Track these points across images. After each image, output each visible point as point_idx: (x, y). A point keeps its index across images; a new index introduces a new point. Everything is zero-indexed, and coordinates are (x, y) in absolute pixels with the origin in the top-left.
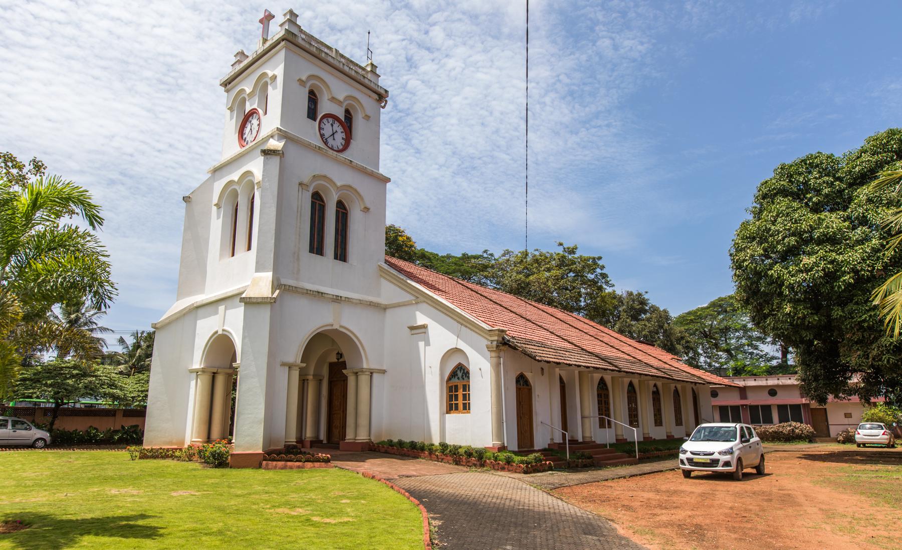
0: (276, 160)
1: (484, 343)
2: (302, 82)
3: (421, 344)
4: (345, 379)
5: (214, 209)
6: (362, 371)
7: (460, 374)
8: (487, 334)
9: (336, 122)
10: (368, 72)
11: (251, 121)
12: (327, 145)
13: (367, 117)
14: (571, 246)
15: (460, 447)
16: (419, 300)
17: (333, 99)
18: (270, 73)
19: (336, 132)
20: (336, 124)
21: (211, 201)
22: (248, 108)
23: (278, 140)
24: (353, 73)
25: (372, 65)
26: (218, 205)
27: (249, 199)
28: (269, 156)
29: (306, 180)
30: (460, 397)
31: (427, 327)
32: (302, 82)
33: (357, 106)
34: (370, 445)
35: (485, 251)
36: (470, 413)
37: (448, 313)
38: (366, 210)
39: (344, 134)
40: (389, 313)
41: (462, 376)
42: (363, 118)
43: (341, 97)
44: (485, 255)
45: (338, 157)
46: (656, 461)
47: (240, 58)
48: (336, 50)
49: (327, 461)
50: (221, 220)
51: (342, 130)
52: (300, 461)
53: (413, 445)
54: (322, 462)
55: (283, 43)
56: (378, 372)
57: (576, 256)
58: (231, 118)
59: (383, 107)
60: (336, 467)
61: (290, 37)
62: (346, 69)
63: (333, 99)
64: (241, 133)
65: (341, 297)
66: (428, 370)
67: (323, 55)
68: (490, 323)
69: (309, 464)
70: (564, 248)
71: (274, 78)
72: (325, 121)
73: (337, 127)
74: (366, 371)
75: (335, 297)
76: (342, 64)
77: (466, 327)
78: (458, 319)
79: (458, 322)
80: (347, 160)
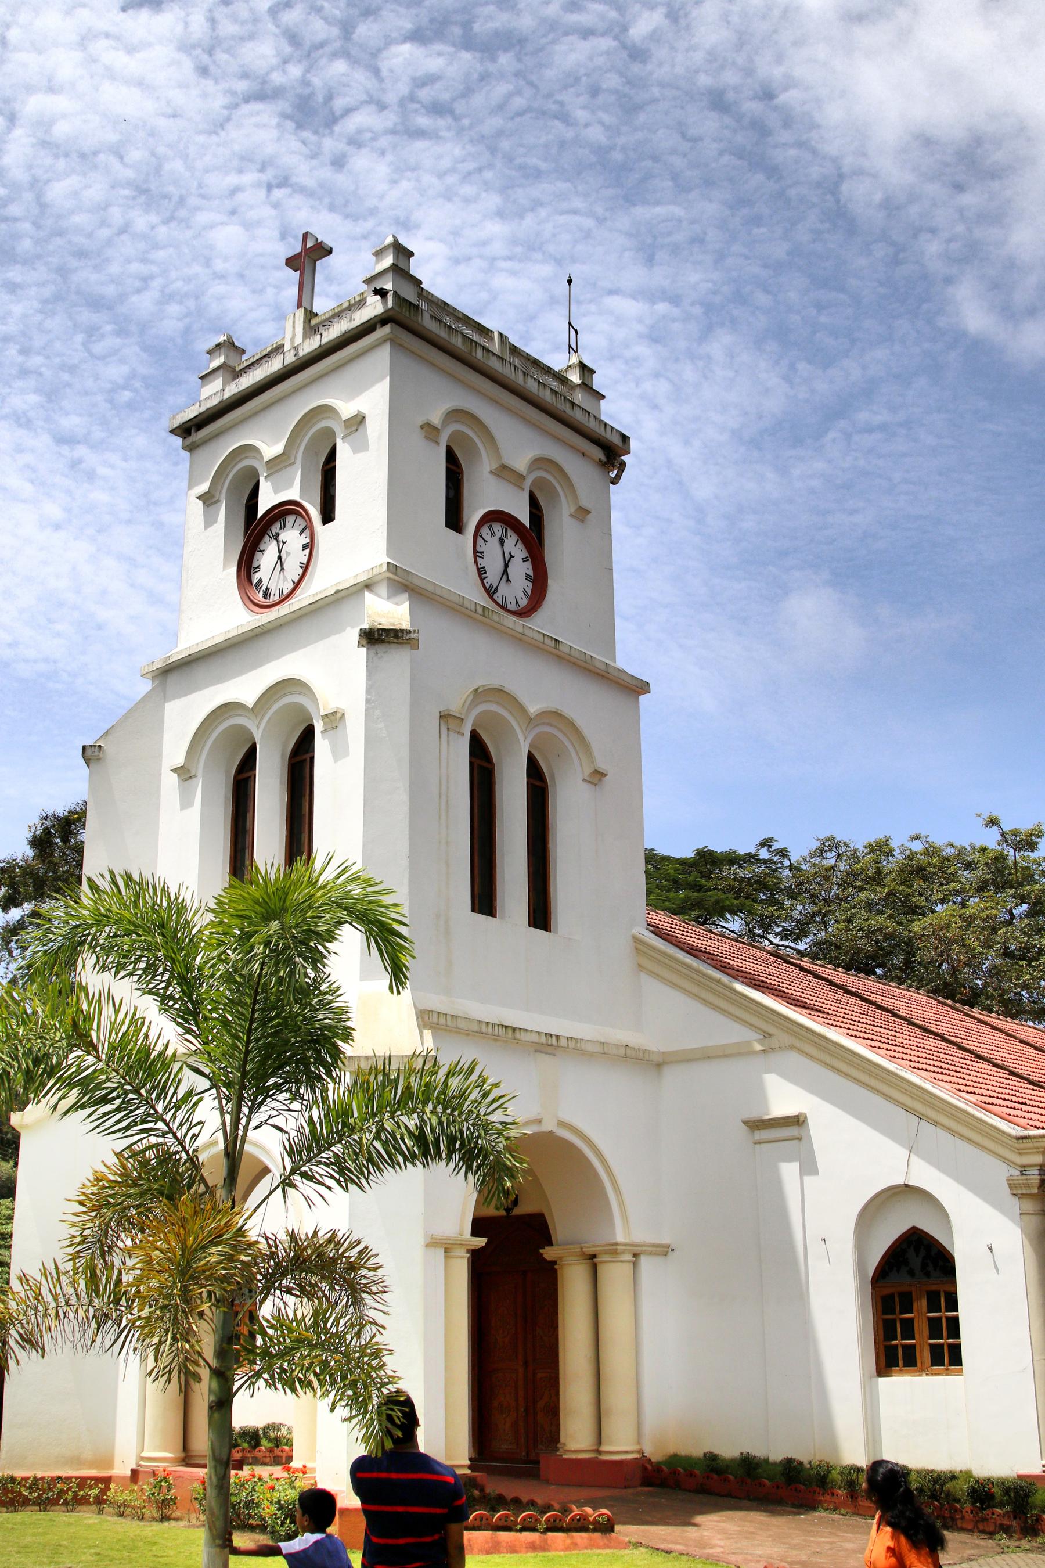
0: (398, 659)
1: (1000, 1173)
2: (430, 431)
3: (789, 1171)
4: (550, 1273)
5: (170, 781)
6: (613, 1250)
7: (916, 1262)
8: (1010, 1148)
9: (510, 532)
10: (573, 387)
11: (278, 535)
12: (492, 598)
13: (582, 514)
14: (1025, 825)
15: (953, 1477)
16: (773, 1042)
17: (504, 472)
18: (346, 409)
19: (511, 556)
20: (511, 540)
21: (158, 756)
22: (265, 502)
23: (389, 598)
24: (547, 396)
25: (583, 367)
26: (184, 773)
27: (283, 755)
28: (380, 648)
29: (455, 706)
30: (921, 1328)
31: (805, 1121)
32: (430, 431)
33: (557, 485)
34: (645, 1468)
35: (766, 843)
36: (960, 1373)
37: (873, 1082)
38: (597, 776)
39: (529, 564)
40: (672, 1076)
41: (924, 1266)
42: (571, 515)
43: (521, 463)
44: (764, 854)
45: (528, 632)
46: (715, 1512)
47: (227, 357)
48: (501, 334)
49: (606, 1528)
50: (195, 811)
51: (525, 554)
52: (534, 1529)
53: (791, 1470)
54: (595, 1530)
55: (387, 329)
56: (651, 1253)
57: (1034, 855)
58: (209, 522)
59: (615, 481)
60: (638, 1545)
61: (405, 314)
62: (532, 386)
63: (504, 472)
64: (246, 566)
65: (557, 1037)
66: (815, 1249)
67: (479, 354)
68: (1021, 1121)
69: (557, 1538)
70: (1003, 834)
71: (358, 421)
72: (485, 531)
73: (514, 546)
74: (623, 1252)
75: (543, 1039)
76: (521, 374)
77: (936, 1123)
78: (908, 1101)
79: (908, 1110)
80: (548, 641)
